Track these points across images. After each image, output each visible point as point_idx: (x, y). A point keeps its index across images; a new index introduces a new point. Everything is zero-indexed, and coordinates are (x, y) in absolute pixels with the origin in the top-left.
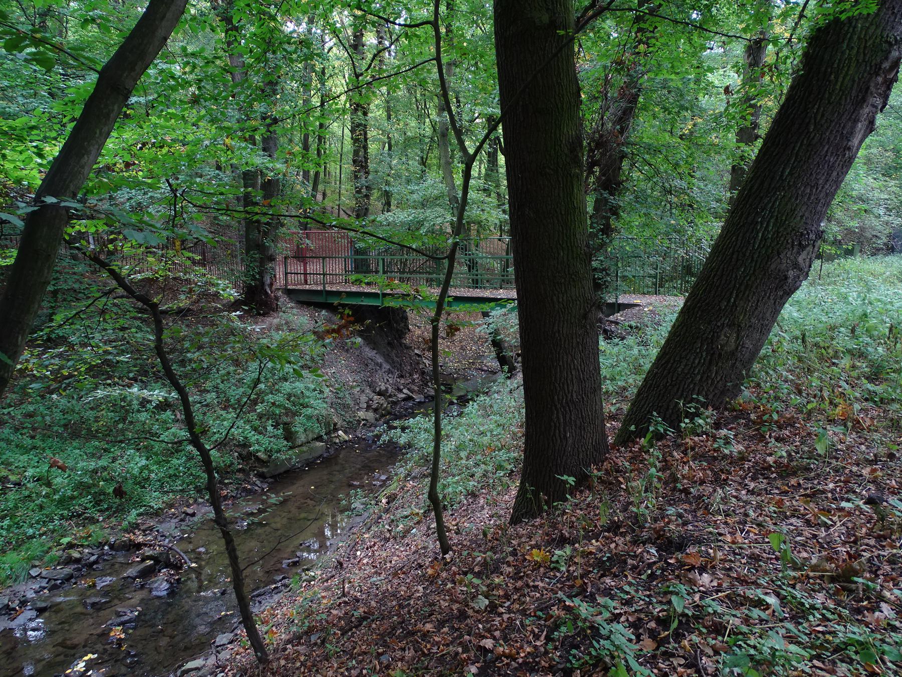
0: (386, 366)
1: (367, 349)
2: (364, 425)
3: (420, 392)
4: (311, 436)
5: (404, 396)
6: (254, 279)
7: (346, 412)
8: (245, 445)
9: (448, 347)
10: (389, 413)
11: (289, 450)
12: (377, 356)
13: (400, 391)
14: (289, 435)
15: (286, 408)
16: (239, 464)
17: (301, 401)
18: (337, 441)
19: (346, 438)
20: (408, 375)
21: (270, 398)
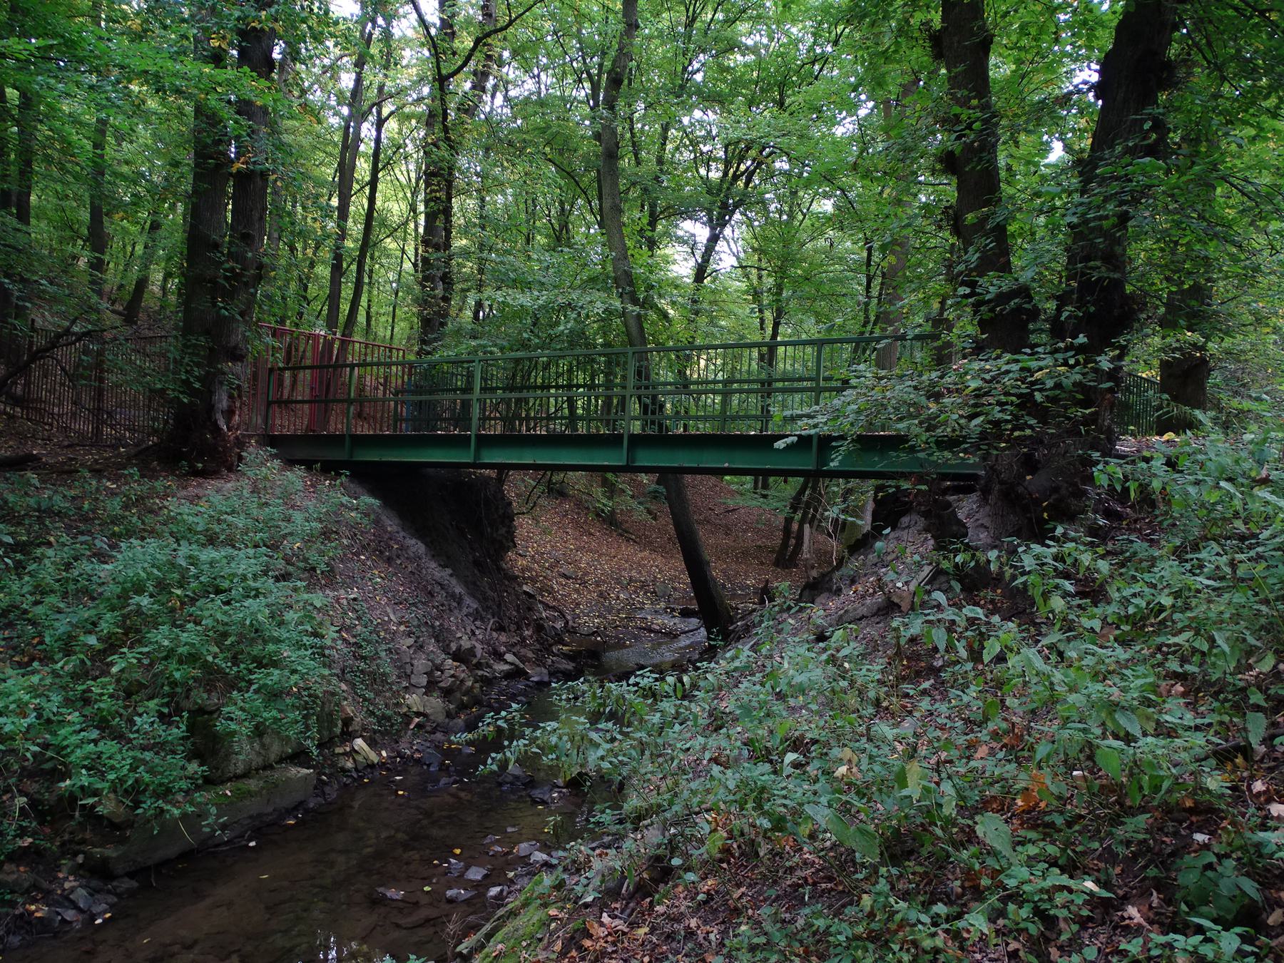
0: (471, 603)
1: (433, 565)
2: (419, 726)
3: (539, 662)
4: (276, 749)
5: (506, 667)
6: (193, 392)
7: (378, 694)
8: (51, 768)
9: (577, 591)
10: (477, 702)
11: (198, 788)
12: (454, 581)
13: (499, 657)
14: (206, 743)
15: (206, 666)
16: (22, 832)
17: (256, 650)
18: (350, 764)
19: (374, 757)
20: (513, 627)
21: (162, 636)
